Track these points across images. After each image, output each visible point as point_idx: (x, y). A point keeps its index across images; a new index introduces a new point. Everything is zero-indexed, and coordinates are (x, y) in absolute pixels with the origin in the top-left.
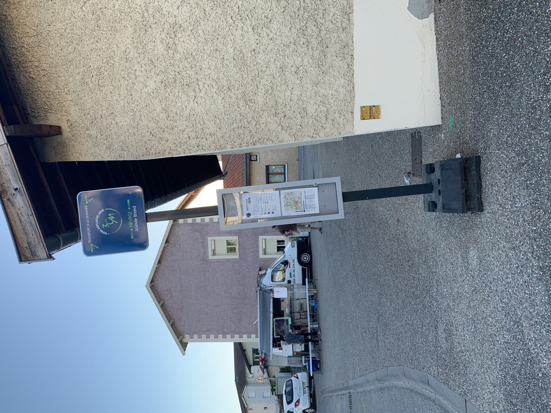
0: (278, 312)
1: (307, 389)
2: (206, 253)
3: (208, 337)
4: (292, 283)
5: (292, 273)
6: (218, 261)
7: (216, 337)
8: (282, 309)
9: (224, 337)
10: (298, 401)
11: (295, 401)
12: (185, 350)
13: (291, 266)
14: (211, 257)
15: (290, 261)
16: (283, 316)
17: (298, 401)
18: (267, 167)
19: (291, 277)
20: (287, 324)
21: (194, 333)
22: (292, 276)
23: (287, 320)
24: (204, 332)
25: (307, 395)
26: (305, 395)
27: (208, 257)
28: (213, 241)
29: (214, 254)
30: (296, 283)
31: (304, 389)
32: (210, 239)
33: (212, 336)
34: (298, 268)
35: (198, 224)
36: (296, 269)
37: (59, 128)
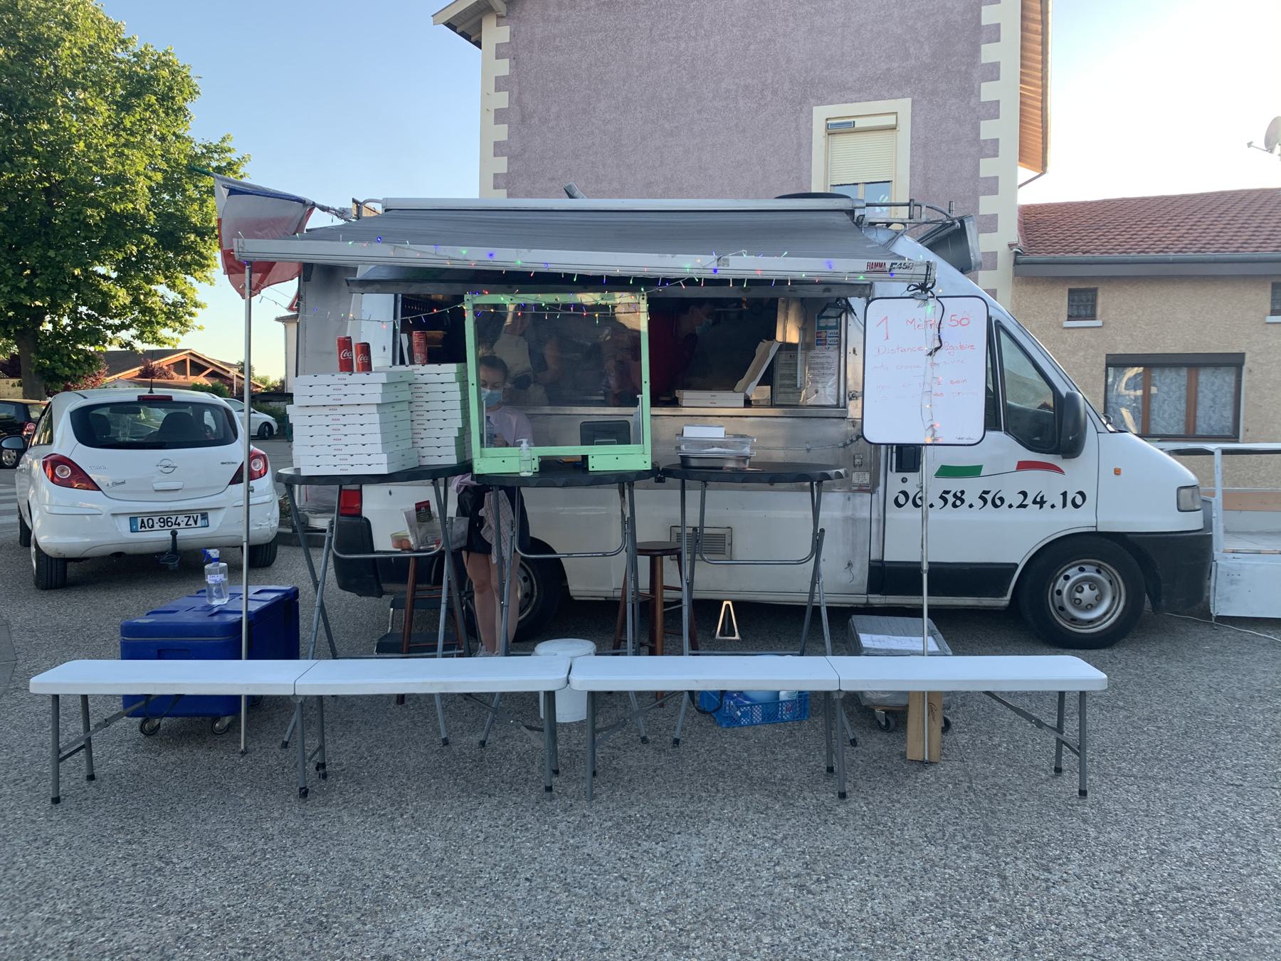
0: (712, 335)
1: (158, 537)
2: (842, 92)
3: (500, 116)
4: (895, 482)
5: (972, 488)
6: (803, 147)
7: (499, 149)
8: (687, 396)
9: (499, 149)
10: (80, 478)
11: (85, 457)
12: (449, 25)
13: (1035, 482)
14: (821, 114)
15: (1076, 474)
16: (654, 403)
17: (80, 478)
18: (1234, 362)
19: (945, 472)
20: (595, 433)
21: (516, 61)
22: (954, 485)
23: (620, 433)
24: (517, 101)
25: (119, 535)
26: (124, 524)
27: (822, 101)
28: (890, 121)
29: (836, 129)
30: (893, 513)
31: (166, 519)
32: (903, 106)
33: (502, 132)
34: (1008, 538)
35: (976, 51)
36: (1003, 514)
37: (344, 585)
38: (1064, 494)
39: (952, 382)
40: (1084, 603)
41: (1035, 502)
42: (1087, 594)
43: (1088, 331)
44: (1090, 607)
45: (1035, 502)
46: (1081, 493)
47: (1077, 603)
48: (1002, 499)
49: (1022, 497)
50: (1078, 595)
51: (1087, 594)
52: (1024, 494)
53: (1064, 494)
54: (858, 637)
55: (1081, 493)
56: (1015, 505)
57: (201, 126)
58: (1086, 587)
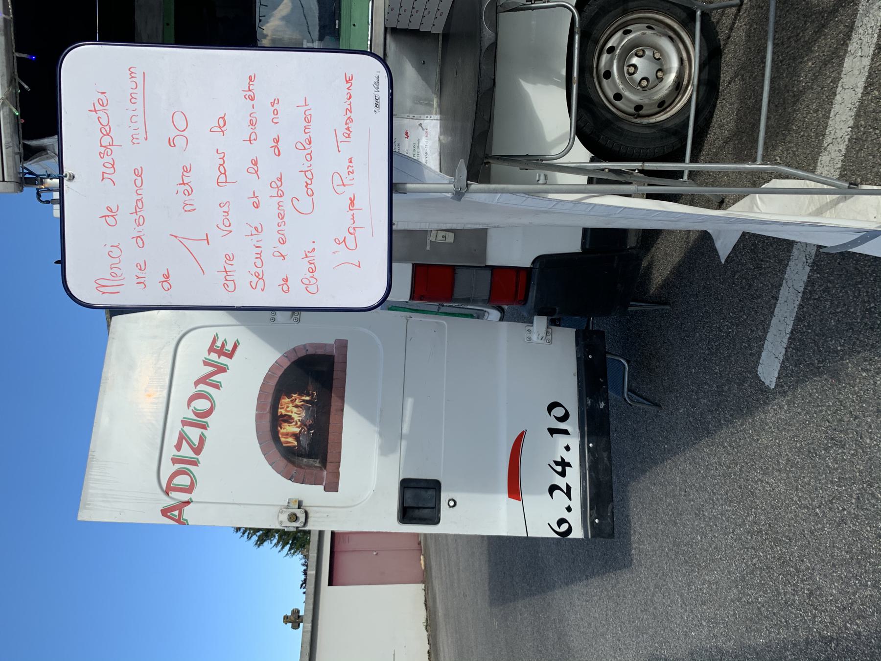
38: (553, 431)
39: (186, 170)
40: (652, 78)
41: (563, 474)
42: (642, 65)
43: (341, 559)
44: (662, 70)
45: (563, 474)
46: (552, 407)
47: (645, 86)
48: (561, 522)
49: (557, 493)
50: (638, 77)
51: (642, 65)
52: (553, 488)
53: (553, 431)
54: (520, 84)
55: (552, 407)
56: (566, 502)
57: (289, 614)
58: (635, 60)
